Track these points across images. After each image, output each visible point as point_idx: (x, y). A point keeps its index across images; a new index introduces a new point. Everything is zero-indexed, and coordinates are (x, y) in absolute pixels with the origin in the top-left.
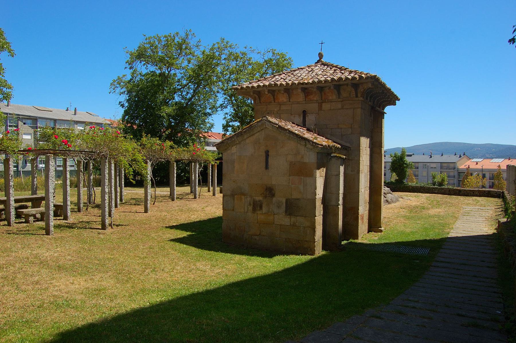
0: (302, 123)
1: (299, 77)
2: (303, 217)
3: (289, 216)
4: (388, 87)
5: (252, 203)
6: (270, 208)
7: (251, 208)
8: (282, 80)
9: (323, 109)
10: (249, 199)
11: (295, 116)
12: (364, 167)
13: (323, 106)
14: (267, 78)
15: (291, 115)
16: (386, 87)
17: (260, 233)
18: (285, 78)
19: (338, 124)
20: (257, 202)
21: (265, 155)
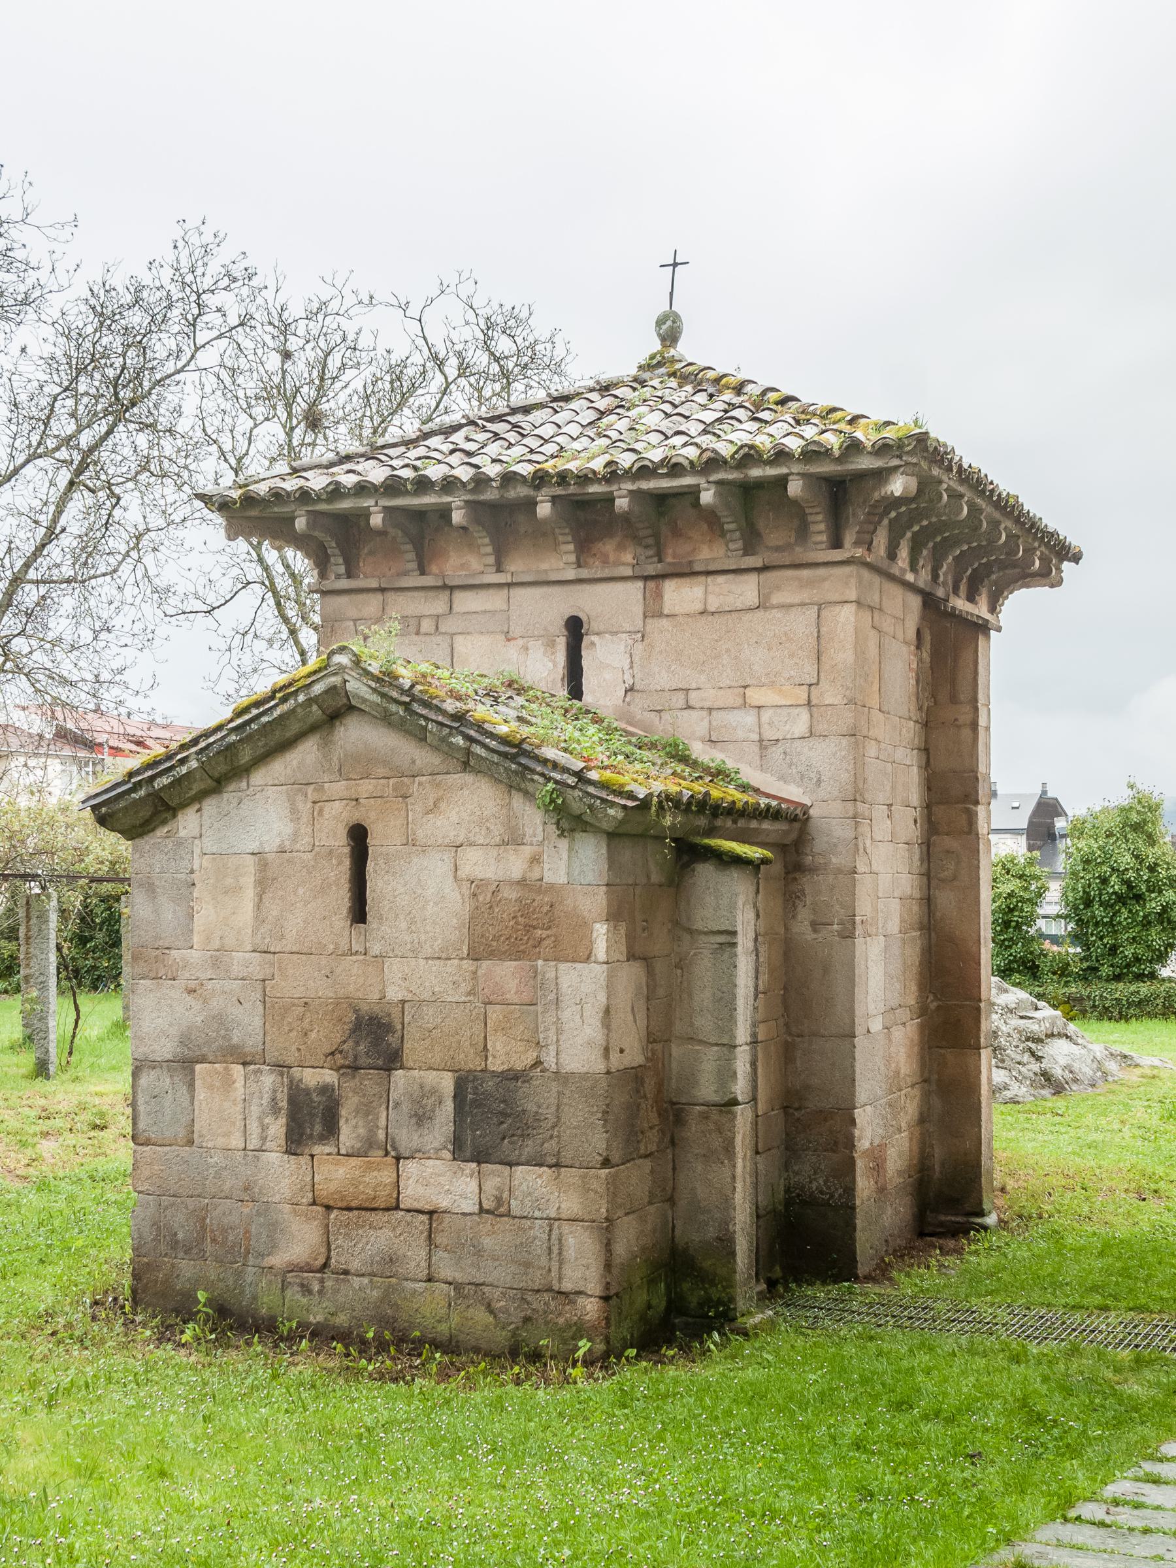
0: (563, 680)
1: (546, 441)
2: (545, 1168)
3: (474, 1165)
4: (1004, 494)
5: (284, 1104)
7: (277, 1128)
8: (455, 459)
9: (666, 612)
11: (526, 649)
12: (881, 906)
13: (666, 597)
14: (383, 447)
15: (509, 640)
16: (992, 491)
18: (470, 446)
19: (745, 687)
20: (307, 1092)
21: (347, 850)
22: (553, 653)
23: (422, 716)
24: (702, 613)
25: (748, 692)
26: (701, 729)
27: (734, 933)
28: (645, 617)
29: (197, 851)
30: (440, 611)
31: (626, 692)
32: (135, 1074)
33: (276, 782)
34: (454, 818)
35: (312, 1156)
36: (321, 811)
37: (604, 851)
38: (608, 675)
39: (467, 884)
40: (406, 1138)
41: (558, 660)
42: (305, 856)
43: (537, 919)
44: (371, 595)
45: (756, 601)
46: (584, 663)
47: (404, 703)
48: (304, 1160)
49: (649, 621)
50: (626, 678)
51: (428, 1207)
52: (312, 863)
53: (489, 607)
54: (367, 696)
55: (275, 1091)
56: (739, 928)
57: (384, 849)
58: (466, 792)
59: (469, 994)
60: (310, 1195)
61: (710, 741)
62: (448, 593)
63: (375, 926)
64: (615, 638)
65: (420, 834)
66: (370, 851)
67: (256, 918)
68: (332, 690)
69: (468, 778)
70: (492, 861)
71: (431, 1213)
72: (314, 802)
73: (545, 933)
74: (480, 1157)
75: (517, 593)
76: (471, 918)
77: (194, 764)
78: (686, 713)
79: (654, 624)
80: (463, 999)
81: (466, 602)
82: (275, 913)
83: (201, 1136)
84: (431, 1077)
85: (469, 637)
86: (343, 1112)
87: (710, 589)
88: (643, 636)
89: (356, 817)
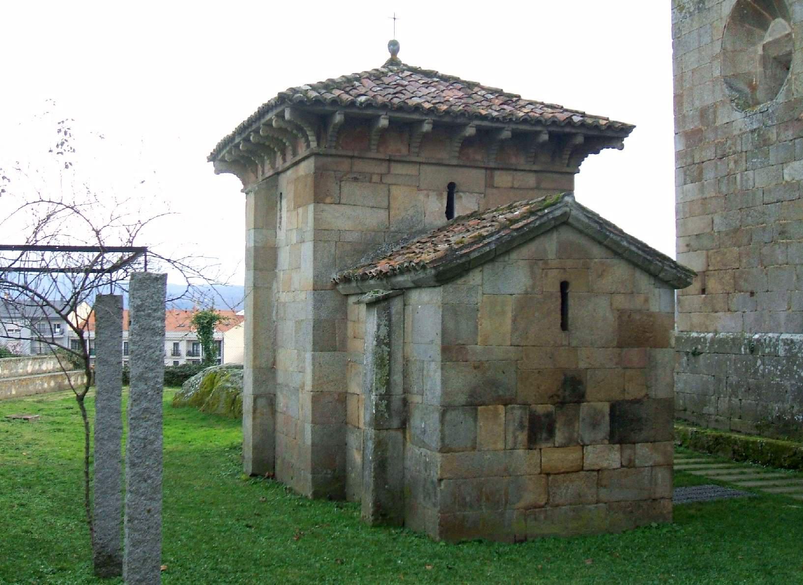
2: (649, 443)
5: (526, 424)
6: (574, 431)
7: (523, 437)
9: (495, 185)
10: (518, 413)
11: (428, 196)
17: (548, 500)
20: (539, 417)
23: (608, 230)
28: (486, 186)
29: (480, 292)
30: (383, 172)
32: (443, 414)
33: (524, 258)
35: (540, 449)
36: (546, 275)
40: (587, 437)
48: (536, 452)
51: (597, 468)
53: (409, 172)
55: (522, 417)
59: (617, 364)
60: (539, 470)
64: (471, 195)
71: (598, 471)
73: (651, 335)
74: (621, 442)
77: (493, 246)
79: (490, 191)
80: (614, 367)
81: (398, 169)
83: (481, 444)
84: (599, 405)
86: (558, 425)
88: (485, 196)
89: (564, 277)
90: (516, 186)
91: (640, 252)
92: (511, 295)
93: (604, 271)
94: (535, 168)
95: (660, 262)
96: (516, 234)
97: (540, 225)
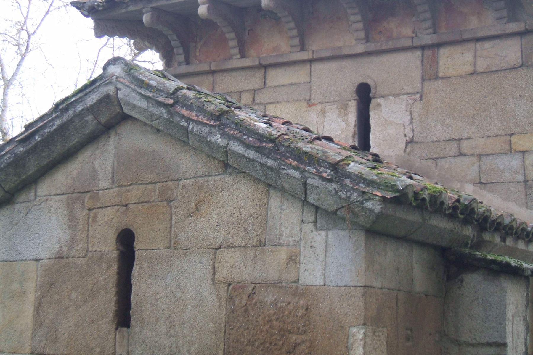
0: (354, 136)
9: (441, 74)
11: (324, 112)
13: (441, 62)
15: (310, 106)
19: (511, 135)
21: (115, 255)
22: (346, 115)
23: (183, 117)
24: (472, 74)
25: (514, 139)
26: (473, 172)
27: (505, 345)
28: (423, 80)
30: (256, 86)
31: (407, 143)
33: (59, 192)
34: (214, 219)
36: (95, 217)
37: (362, 250)
38: (391, 130)
39: (223, 287)
41: (350, 120)
42: (79, 261)
43: (292, 323)
44: (204, 77)
45: (520, 61)
46: (372, 122)
47: (165, 106)
49: (426, 83)
50: (406, 132)
52: (85, 267)
53: (295, 80)
54: (135, 102)
56: (509, 340)
57: (147, 253)
58: (226, 194)
61: (481, 183)
62: (262, 71)
63: (137, 329)
64: (397, 99)
65: (182, 236)
66: (136, 256)
67: (35, 321)
68: (106, 99)
69: (228, 179)
70: (249, 262)
72: (90, 210)
75: (318, 67)
76: (227, 322)
78: (459, 160)
82: (51, 317)
85: (278, 105)
87: (478, 53)
88: (421, 96)
90: (480, 69)
91: (251, 154)
92: (36, 260)
93: (202, 201)
94: (513, 27)
95: (296, 168)
96: (21, 149)
97: (63, 127)
